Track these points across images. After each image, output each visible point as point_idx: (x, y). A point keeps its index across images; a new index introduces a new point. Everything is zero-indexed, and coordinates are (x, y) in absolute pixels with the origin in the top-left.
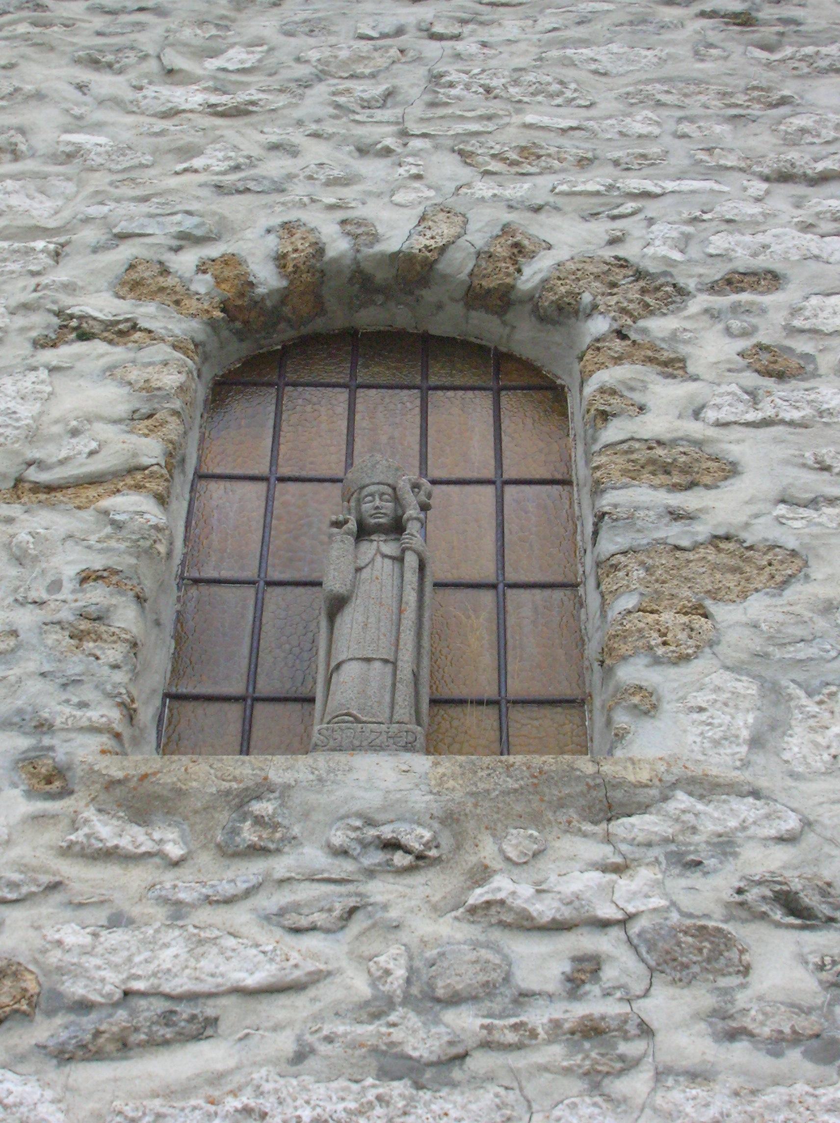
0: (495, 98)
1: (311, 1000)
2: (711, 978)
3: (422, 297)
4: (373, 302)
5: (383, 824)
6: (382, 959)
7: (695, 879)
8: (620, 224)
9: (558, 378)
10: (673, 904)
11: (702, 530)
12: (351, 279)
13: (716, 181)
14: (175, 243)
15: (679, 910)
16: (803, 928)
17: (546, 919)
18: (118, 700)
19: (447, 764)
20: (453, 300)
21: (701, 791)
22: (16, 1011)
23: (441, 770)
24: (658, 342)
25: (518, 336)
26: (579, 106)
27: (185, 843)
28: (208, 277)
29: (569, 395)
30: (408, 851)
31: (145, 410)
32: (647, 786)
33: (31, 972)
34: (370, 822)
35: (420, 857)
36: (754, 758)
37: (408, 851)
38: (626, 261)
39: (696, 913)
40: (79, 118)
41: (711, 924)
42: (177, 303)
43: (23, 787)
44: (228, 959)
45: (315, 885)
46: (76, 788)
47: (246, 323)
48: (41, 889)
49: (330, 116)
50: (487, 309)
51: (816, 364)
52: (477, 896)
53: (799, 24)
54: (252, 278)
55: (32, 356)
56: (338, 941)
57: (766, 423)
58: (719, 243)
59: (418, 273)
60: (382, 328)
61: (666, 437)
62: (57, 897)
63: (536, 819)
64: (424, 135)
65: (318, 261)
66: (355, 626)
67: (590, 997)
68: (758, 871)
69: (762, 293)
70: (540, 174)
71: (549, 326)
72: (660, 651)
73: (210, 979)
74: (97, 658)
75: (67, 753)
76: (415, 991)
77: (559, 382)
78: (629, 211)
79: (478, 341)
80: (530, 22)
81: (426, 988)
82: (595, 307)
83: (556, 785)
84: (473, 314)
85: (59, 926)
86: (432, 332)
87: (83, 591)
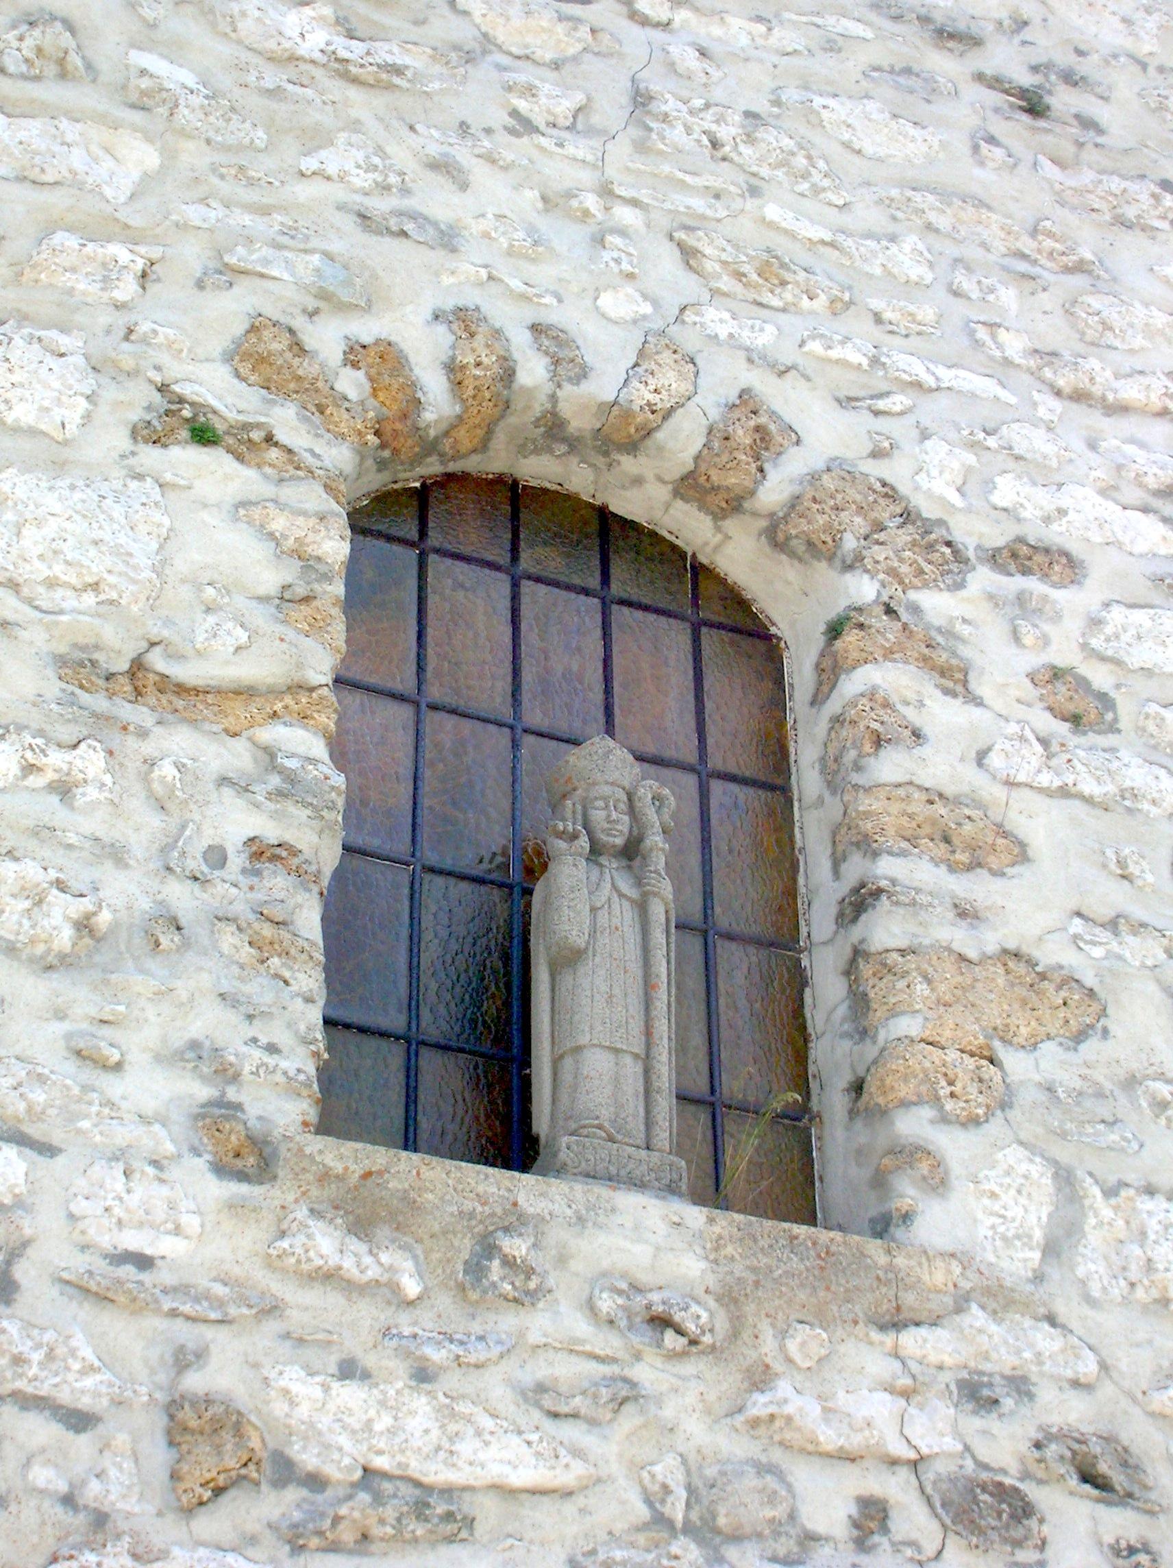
0: (724, 159)
1: (580, 1510)
2: (1009, 1549)
3: (619, 463)
4: (551, 451)
5: (651, 1290)
6: (657, 1469)
7: (990, 1421)
8: (882, 424)
9: (774, 624)
10: (967, 1448)
11: (991, 940)
12: (538, 420)
13: (1001, 383)
14: (312, 304)
15: (974, 1457)
16: (1098, 1500)
17: (829, 1448)
18: (313, 1047)
19: (724, 1223)
20: (660, 479)
21: (995, 1305)
22: (245, 1477)
23: (717, 1229)
24: (933, 633)
25: (729, 549)
26: (830, 204)
27: (421, 1277)
28: (360, 375)
29: (785, 654)
30: (680, 1332)
31: (301, 591)
32: (939, 1292)
33: (256, 1428)
34: (637, 1288)
35: (693, 1342)
36: (1048, 1270)
37: (680, 1332)
38: (893, 489)
39: (993, 1465)
40: (153, 26)
41: (1008, 1481)
42: (321, 409)
43: (208, 1157)
44: (487, 1444)
45: (574, 1359)
46: (281, 1173)
47: (396, 452)
48: (254, 1311)
49: (505, 128)
50: (703, 507)
51: (1115, 713)
52: (760, 1405)
53: (1100, 131)
54: (419, 394)
55: (133, 453)
56: (605, 1437)
57: (1064, 792)
58: (1007, 491)
59: (630, 436)
60: (548, 486)
61: (950, 791)
62: (273, 1326)
63: (821, 1318)
64: (634, 203)
65: (505, 387)
66: (597, 997)
67: (880, 1550)
68: (1055, 1420)
69: (1054, 585)
70: (784, 310)
71: (784, 557)
72: (949, 1105)
73: (468, 1469)
74: (286, 982)
75: (260, 1118)
76: (694, 1516)
77: (773, 630)
78: (898, 408)
79: (672, 538)
80: (762, 28)
81: (707, 1516)
82: (859, 558)
83: (843, 1271)
84: (679, 504)
85: (280, 1367)
86: (612, 508)
87: (258, 873)
